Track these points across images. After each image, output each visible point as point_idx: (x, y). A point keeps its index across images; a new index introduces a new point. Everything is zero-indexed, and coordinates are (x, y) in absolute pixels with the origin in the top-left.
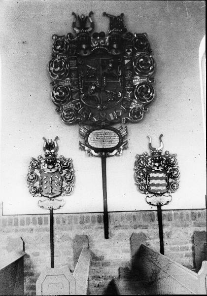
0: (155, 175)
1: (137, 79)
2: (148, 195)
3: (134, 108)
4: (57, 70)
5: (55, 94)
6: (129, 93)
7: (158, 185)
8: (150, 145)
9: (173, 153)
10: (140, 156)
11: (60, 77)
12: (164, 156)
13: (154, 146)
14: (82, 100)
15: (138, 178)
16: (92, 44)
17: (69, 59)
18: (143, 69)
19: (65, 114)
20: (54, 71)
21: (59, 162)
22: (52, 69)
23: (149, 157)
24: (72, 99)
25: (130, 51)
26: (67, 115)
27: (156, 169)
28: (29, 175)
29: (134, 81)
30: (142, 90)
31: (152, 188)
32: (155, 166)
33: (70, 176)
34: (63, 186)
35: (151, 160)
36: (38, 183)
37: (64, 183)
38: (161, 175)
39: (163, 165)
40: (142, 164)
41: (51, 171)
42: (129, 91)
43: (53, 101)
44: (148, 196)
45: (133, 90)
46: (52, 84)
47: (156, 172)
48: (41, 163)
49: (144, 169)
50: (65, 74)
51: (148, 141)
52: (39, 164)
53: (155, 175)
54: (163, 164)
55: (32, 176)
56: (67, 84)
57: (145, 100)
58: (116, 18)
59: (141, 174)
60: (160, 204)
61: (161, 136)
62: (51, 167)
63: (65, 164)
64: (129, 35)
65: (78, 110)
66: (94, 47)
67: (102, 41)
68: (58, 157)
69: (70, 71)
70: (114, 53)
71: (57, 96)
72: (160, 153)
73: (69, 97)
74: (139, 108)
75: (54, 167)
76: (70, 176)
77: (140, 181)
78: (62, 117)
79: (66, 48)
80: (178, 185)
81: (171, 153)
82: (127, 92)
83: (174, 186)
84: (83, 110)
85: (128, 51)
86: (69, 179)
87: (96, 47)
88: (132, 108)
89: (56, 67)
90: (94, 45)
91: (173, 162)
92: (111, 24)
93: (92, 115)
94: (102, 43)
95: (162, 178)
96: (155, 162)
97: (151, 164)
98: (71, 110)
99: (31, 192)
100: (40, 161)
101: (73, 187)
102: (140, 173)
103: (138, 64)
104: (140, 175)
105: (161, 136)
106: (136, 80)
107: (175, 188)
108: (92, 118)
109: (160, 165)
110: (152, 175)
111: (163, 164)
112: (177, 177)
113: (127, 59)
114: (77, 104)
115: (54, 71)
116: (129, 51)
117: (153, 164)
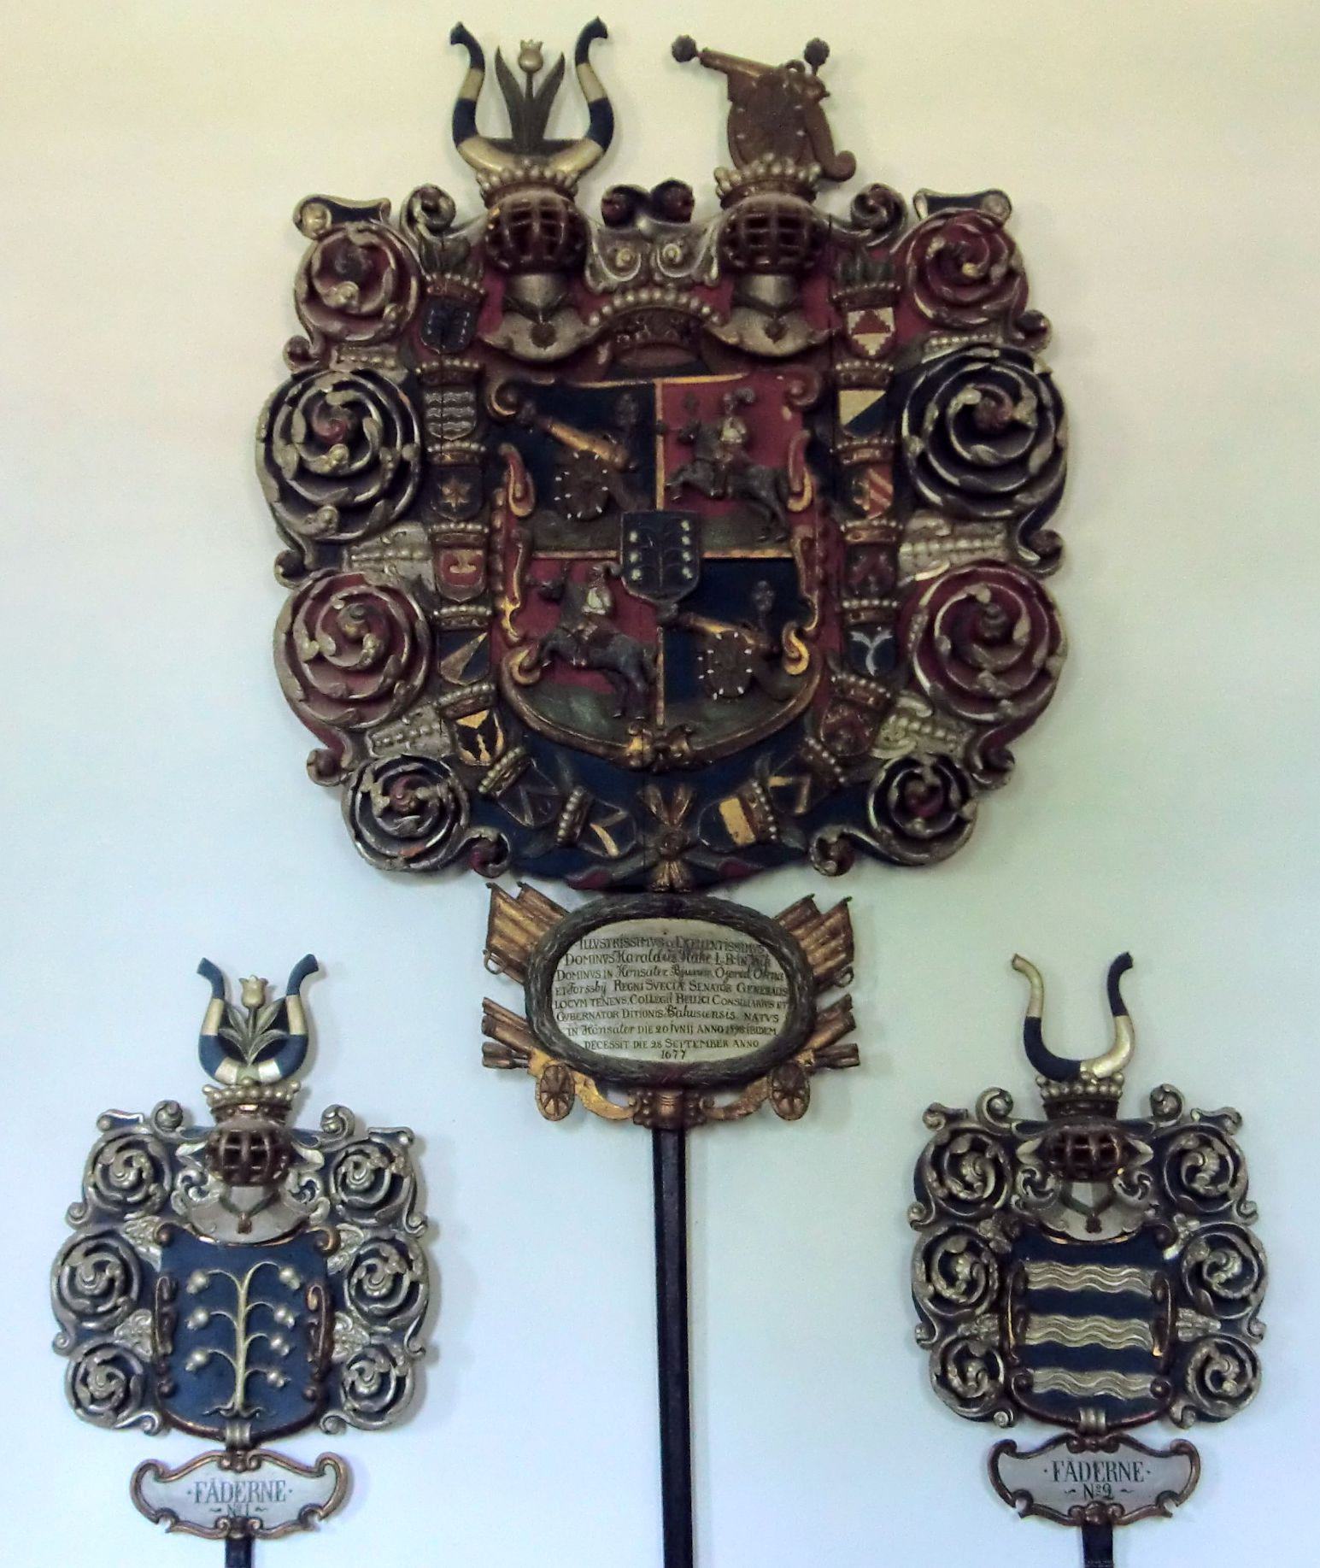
0: (1077, 1278)
1: (928, 535)
2: (1015, 1434)
3: (908, 762)
4: (323, 464)
5: (307, 648)
6: (873, 644)
7: (1093, 1358)
8: (1033, 1030)
9: (1213, 1106)
10: (953, 1117)
11: (350, 513)
12: (1139, 1127)
13: (1062, 1043)
14: (513, 694)
15: (937, 1298)
16: (596, 273)
17: (415, 385)
18: (977, 467)
19: (381, 802)
20: (303, 472)
21: (315, 1156)
22: (288, 457)
23: (1027, 1127)
24: (434, 684)
25: (881, 327)
26: (389, 812)
27: (1078, 1230)
28: (77, 1254)
29: (905, 549)
30: (964, 623)
31: (1044, 1379)
32: (1066, 1201)
33: (378, 1173)
34: (338, 1354)
35: (1039, 1153)
36: (144, 1320)
37: (345, 1325)
38: (1120, 1279)
39: (1133, 1200)
40: (968, 1186)
41: (245, 1228)
42: (869, 629)
43: (290, 700)
44: (1008, 1447)
45: (898, 621)
46: (291, 569)
47: (1078, 1254)
48: (176, 1166)
49: (986, 1229)
50: (391, 493)
51: (1097, 1053)
52: (157, 1176)
53: (1077, 1278)
54: (1131, 1188)
55: (100, 1267)
56: (405, 568)
57: (990, 702)
58: (771, 79)
59: (963, 1268)
60: (1102, 1507)
61: (1123, 964)
62: (247, 1196)
63: (360, 1179)
64: (873, 211)
65: (483, 771)
66: (608, 293)
67: (674, 250)
68: (307, 1119)
69: (430, 473)
70: (757, 338)
71: (319, 660)
72: (1107, 1105)
73: (406, 673)
74: (944, 760)
75: (272, 1201)
76: (397, 1278)
77: (949, 1326)
78: (359, 819)
79: (399, 295)
80: (1250, 1367)
81: (1202, 1098)
82: (858, 636)
83: (1219, 1378)
84: (523, 772)
85: (865, 327)
86: (368, 1191)
87: (623, 289)
88: (895, 756)
89: (318, 444)
90: (614, 279)
91: (1216, 1179)
92: (735, 125)
93: (589, 812)
94: (671, 264)
95: (1120, 1306)
96: (1070, 1176)
97: (1038, 1188)
98: (428, 771)
99: (83, 1394)
100: (171, 1147)
101: (411, 1360)
102: (948, 1258)
103: (941, 423)
104: (951, 1280)
105: (1123, 964)
106: (921, 547)
107: (1229, 1386)
108: (588, 832)
109: (1109, 1202)
110: (1041, 1276)
111: (1131, 1188)
112: (1245, 1301)
113: (861, 385)
114: (475, 721)
115: (303, 472)
116: (876, 326)
117: (1051, 1183)
